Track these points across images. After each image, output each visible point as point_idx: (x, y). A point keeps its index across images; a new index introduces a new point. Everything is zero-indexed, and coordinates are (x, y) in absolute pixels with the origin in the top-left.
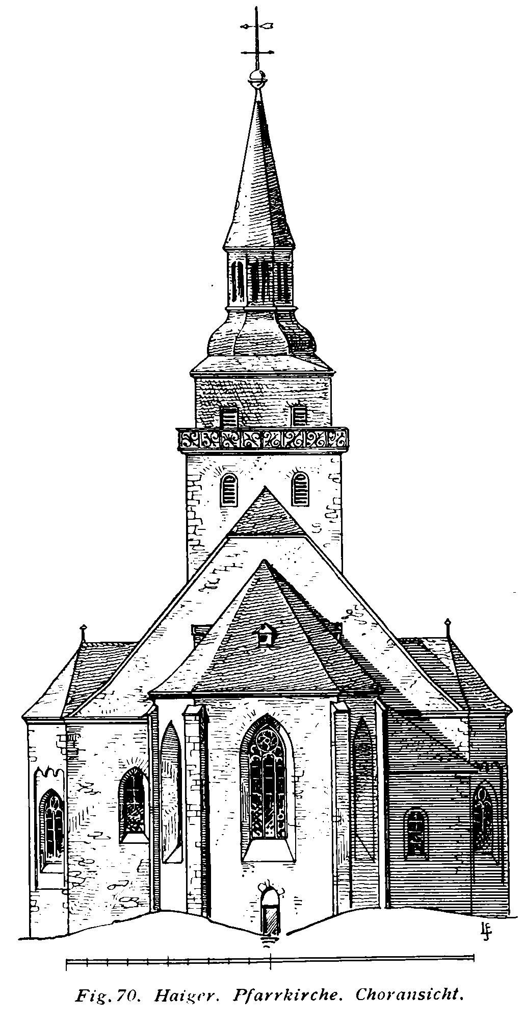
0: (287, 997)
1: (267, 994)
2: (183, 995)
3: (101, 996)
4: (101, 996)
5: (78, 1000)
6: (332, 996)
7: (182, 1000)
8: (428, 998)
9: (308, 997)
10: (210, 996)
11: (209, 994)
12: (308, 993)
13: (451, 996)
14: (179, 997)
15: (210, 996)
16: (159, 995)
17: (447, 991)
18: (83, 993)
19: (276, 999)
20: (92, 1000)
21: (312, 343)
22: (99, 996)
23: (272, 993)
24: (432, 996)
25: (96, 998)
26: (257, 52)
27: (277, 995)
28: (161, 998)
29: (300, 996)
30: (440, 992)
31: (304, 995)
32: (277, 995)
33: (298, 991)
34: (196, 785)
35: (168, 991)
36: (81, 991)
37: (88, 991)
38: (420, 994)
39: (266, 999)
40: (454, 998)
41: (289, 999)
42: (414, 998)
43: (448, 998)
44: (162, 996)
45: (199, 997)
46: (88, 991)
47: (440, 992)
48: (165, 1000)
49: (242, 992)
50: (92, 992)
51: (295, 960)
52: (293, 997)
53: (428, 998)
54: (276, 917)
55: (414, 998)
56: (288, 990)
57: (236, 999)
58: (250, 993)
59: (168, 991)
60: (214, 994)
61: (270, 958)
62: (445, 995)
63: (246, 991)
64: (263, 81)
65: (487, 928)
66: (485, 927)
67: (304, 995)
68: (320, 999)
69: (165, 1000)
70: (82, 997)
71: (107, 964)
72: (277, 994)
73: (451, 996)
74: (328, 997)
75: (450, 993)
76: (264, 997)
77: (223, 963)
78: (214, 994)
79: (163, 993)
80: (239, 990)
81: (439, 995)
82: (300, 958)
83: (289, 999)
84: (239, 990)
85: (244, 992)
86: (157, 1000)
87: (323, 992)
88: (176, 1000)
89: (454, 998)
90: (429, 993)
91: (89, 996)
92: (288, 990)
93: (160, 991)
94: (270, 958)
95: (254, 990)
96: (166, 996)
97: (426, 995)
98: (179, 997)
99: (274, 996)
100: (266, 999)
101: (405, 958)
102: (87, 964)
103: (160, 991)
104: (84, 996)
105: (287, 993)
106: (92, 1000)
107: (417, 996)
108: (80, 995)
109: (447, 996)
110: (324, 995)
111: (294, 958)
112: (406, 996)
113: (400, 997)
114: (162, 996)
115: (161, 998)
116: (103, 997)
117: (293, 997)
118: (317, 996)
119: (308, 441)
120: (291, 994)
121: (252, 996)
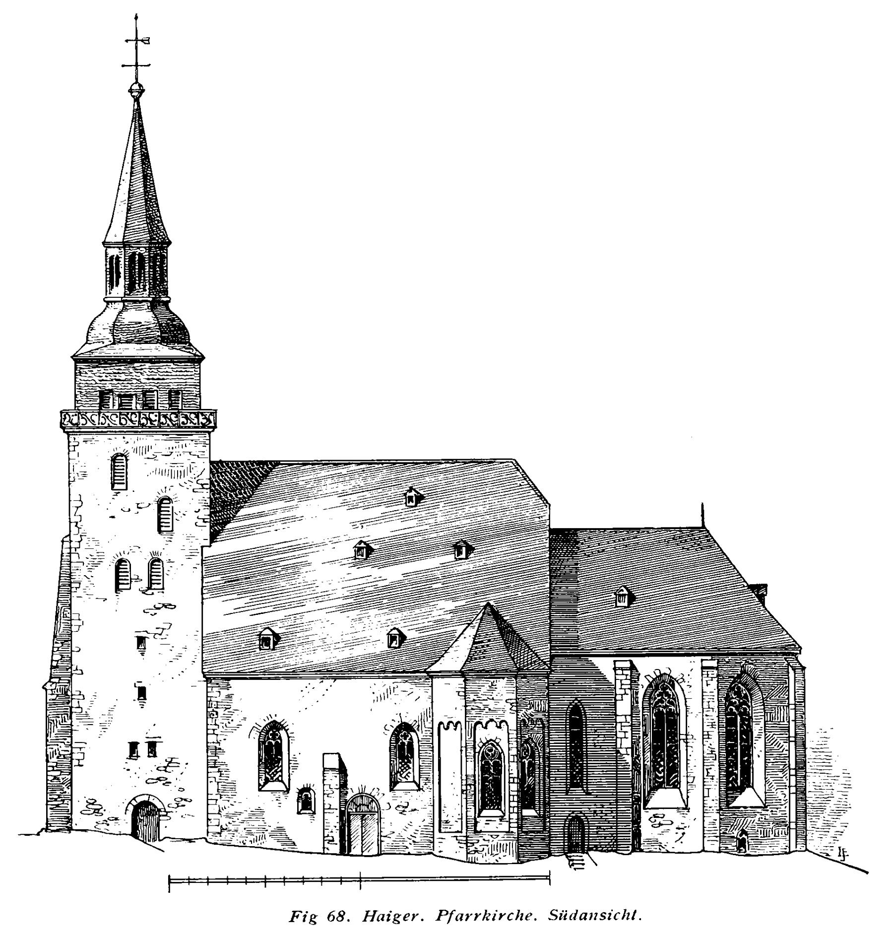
0: (485, 918)
1: (476, 914)
2: (389, 915)
3: (397, 916)
4: (313, 917)
5: (292, 921)
6: (527, 917)
7: (388, 920)
8: (609, 919)
9: (505, 917)
10: (414, 916)
11: (467, 915)
12: (505, 914)
13: (630, 917)
14: (386, 918)
15: (414, 916)
16: (367, 916)
17: (627, 912)
18: (296, 914)
19: (475, 920)
20: (304, 921)
21: (183, 329)
22: (311, 916)
23: (471, 914)
24: (612, 917)
25: (308, 919)
26: (137, 65)
27: (477, 916)
28: (369, 919)
29: (498, 916)
30: (513, 914)
31: (501, 916)
32: (477, 916)
33: (496, 913)
34: (626, 679)
35: (375, 912)
36: (294, 912)
37: (301, 912)
38: (605, 918)
39: (466, 920)
40: (633, 919)
41: (487, 920)
42: (595, 919)
43: (521, 919)
44: (371, 916)
45: (405, 917)
46: (301, 912)
47: (619, 913)
48: (372, 920)
49: (444, 913)
50: (304, 913)
51: (436, 879)
52: (491, 918)
53: (565, 919)
54: (352, 837)
55: (595, 919)
56: (486, 911)
57: (439, 919)
58: (452, 914)
59: (375, 912)
60: (417, 914)
61: (322, 881)
62: (518, 916)
63: (447, 912)
64: (142, 91)
65: (843, 852)
66: (842, 851)
67: (501, 916)
68: (623, 919)
69: (372, 920)
70: (295, 918)
71: (246, 879)
72: (476, 914)
73: (630, 917)
74: (524, 917)
75: (629, 914)
76: (464, 917)
77: (194, 879)
78: (417, 914)
79: (371, 913)
80: (441, 911)
81: (619, 917)
82: (216, 879)
83: (487, 920)
84: (441, 911)
85: (445, 913)
86: (365, 920)
87: (519, 913)
88: (575, 919)
89: (633, 919)
90: (610, 914)
91: (301, 917)
92: (486, 911)
93: (368, 912)
94: (322, 881)
95: (455, 910)
96: (373, 916)
97: (607, 916)
98: (386, 918)
99: (472, 918)
100: (466, 920)
101: (351, 880)
102: (227, 879)
103: (368, 912)
104: (297, 917)
105: (486, 914)
106: (304, 921)
107: (599, 917)
108: (294, 916)
109: (519, 918)
110: (520, 916)
111: (527, 879)
112: (588, 917)
113: (458, 918)
114: (371, 916)
115: (369, 919)
116: (314, 918)
117: (491, 918)
118: (513, 917)
119: (130, 414)
120: (490, 914)
121: (454, 917)
